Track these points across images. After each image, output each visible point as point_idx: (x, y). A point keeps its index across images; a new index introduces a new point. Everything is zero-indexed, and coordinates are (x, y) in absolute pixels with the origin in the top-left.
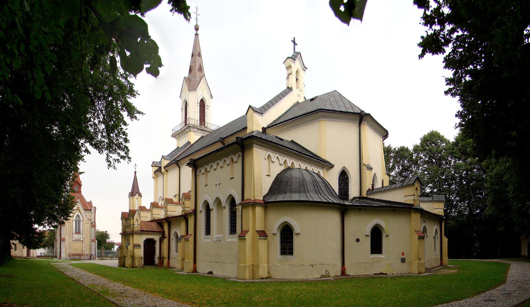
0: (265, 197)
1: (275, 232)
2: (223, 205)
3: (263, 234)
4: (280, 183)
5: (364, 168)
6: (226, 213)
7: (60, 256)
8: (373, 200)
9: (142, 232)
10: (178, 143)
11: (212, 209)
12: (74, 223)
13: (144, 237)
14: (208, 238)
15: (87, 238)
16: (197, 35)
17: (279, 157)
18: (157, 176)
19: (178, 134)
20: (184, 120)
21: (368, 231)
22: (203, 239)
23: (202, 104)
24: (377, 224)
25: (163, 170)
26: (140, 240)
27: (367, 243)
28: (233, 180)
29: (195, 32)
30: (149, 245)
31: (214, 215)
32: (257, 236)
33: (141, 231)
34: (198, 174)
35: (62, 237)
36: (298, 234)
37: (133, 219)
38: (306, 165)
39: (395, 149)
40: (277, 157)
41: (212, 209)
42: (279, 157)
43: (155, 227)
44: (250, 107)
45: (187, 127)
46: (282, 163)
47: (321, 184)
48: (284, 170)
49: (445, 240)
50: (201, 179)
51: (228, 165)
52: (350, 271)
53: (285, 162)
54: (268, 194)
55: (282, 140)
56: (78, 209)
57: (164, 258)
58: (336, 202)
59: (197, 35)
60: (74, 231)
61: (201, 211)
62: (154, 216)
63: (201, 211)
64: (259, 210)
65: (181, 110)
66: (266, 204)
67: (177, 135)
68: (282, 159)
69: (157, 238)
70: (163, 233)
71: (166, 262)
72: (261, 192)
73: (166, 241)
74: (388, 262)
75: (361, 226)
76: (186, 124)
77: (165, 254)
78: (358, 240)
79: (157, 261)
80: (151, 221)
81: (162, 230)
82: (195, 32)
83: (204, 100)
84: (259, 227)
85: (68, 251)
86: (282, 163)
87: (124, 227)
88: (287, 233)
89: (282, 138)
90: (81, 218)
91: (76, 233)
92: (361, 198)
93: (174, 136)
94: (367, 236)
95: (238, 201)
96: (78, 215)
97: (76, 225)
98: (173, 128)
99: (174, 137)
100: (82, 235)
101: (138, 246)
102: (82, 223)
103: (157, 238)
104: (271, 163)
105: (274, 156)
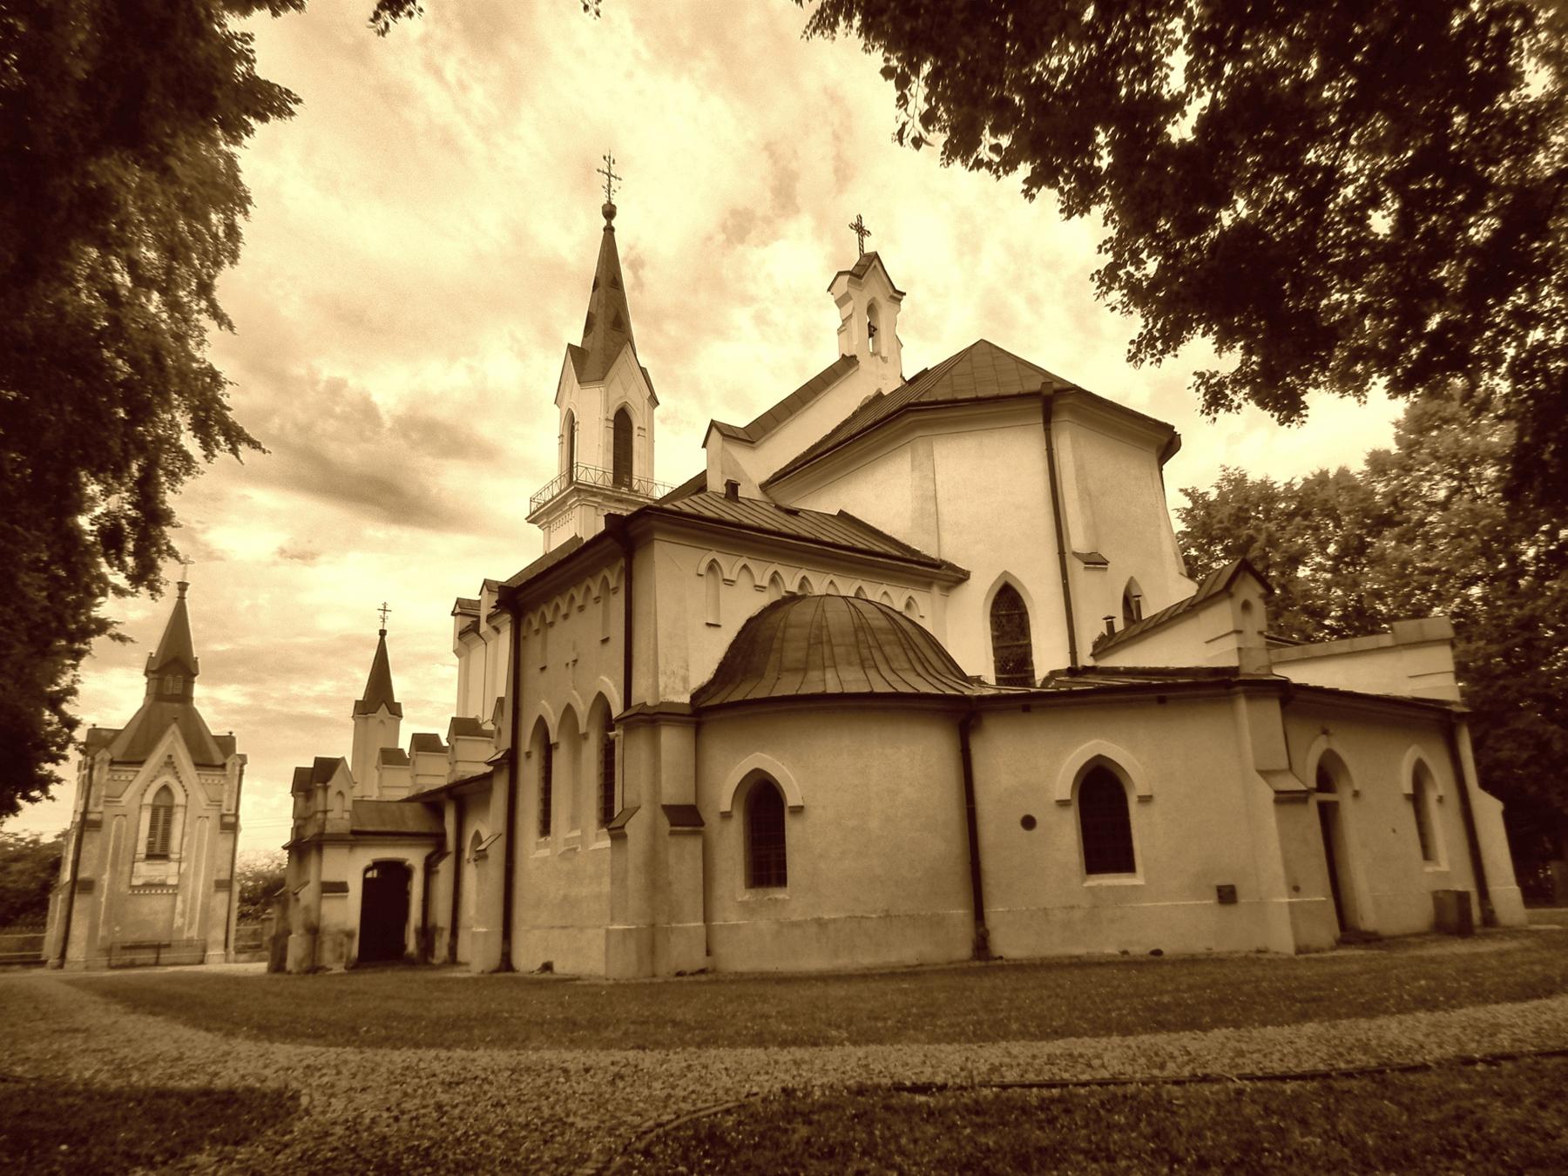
0: (694, 697)
1: (728, 808)
2: (582, 730)
3: (686, 817)
4: (751, 648)
5: (1076, 567)
6: (591, 752)
7: (63, 955)
8: (1114, 672)
9: (357, 838)
10: (548, 540)
11: (556, 745)
12: (146, 817)
13: (367, 856)
14: (547, 845)
15: (196, 874)
16: (609, 230)
17: (750, 564)
18: (467, 645)
19: (548, 513)
20: (565, 468)
21: (1063, 783)
22: (533, 845)
23: (622, 425)
24: (1100, 757)
25: (484, 627)
26: (351, 868)
27: (1065, 834)
28: (610, 644)
29: (604, 222)
30: (386, 888)
31: (560, 760)
32: (664, 824)
33: (354, 833)
34: (524, 633)
35: (82, 875)
36: (798, 810)
37: (326, 789)
38: (858, 583)
39: (1289, 485)
40: (745, 567)
41: (556, 745)
42: (750, 564)
43: (414, 820)
44: (713, 424)
45: (575, 490)
46: (765, 583)
47: (919, 640)
48: (774, 607)
49: (1489, 811)
50: (533, 648)
51: (597, 600)
52: (1009, 943)
53: (775, 579)
54: (711, 683)
55: (793, 513)
56: (170, 763)
57: (435, 928)
58: (925, 688)
59: (609, 230)
60: (142, 849)
61: (528, 755)
62: (421, 781)
63: (528, 755)
64: (672, 741)
65: (558, 441)
66: (706, 713)
67: (542, 515)
68: (762, 572)
69: (414, 857)
70: (438, 839)
71: (441, 951)
72: (685, 680)
73: (445, 867)
74: (1155, 908)
75: (1035, 769)
76: (571, 482)
77: (442, 916)
78: (1029, 822)
79: (412, 944)
80: (408, 800)
81: (435, 830)
82: (604, 222)
83: (629, 409)
84: (674, 791)
85: (102, 932)
86: (765, 583)
87: (301, 821)
88: (764, 805)
89: (796, 505)
90: (179, 798)
91: (151, 856)
92: (1073, 671)
93: (533, 519)
94: (1063, 804)
95: (617, 709)
96: (166, 788)
97: (153, 827)
98: (532, 493)
99: (532, 522)
100: (173, 867)
101: (340, 888)
102: (178, 817)
103: (414, 857)
104: (723, 587)
105: (730, 565)
